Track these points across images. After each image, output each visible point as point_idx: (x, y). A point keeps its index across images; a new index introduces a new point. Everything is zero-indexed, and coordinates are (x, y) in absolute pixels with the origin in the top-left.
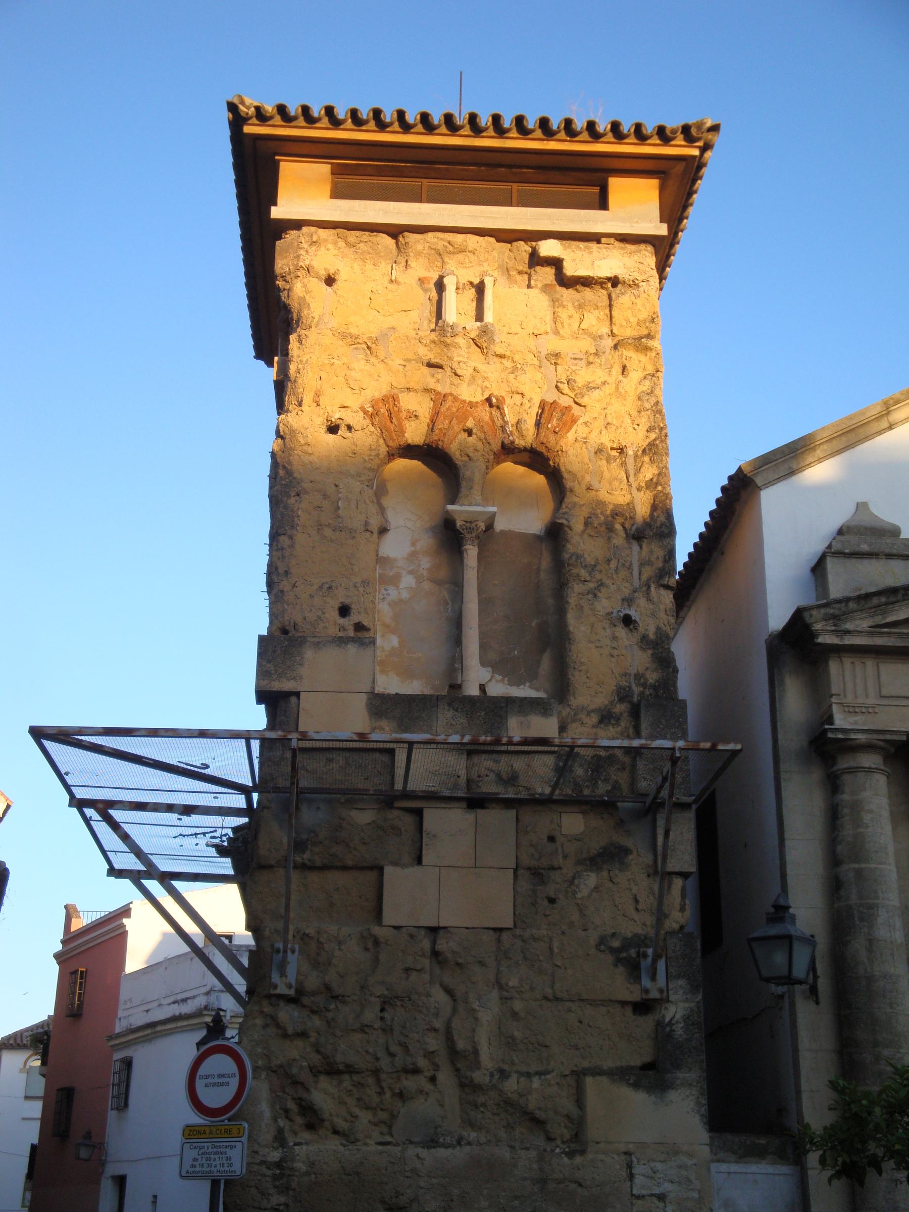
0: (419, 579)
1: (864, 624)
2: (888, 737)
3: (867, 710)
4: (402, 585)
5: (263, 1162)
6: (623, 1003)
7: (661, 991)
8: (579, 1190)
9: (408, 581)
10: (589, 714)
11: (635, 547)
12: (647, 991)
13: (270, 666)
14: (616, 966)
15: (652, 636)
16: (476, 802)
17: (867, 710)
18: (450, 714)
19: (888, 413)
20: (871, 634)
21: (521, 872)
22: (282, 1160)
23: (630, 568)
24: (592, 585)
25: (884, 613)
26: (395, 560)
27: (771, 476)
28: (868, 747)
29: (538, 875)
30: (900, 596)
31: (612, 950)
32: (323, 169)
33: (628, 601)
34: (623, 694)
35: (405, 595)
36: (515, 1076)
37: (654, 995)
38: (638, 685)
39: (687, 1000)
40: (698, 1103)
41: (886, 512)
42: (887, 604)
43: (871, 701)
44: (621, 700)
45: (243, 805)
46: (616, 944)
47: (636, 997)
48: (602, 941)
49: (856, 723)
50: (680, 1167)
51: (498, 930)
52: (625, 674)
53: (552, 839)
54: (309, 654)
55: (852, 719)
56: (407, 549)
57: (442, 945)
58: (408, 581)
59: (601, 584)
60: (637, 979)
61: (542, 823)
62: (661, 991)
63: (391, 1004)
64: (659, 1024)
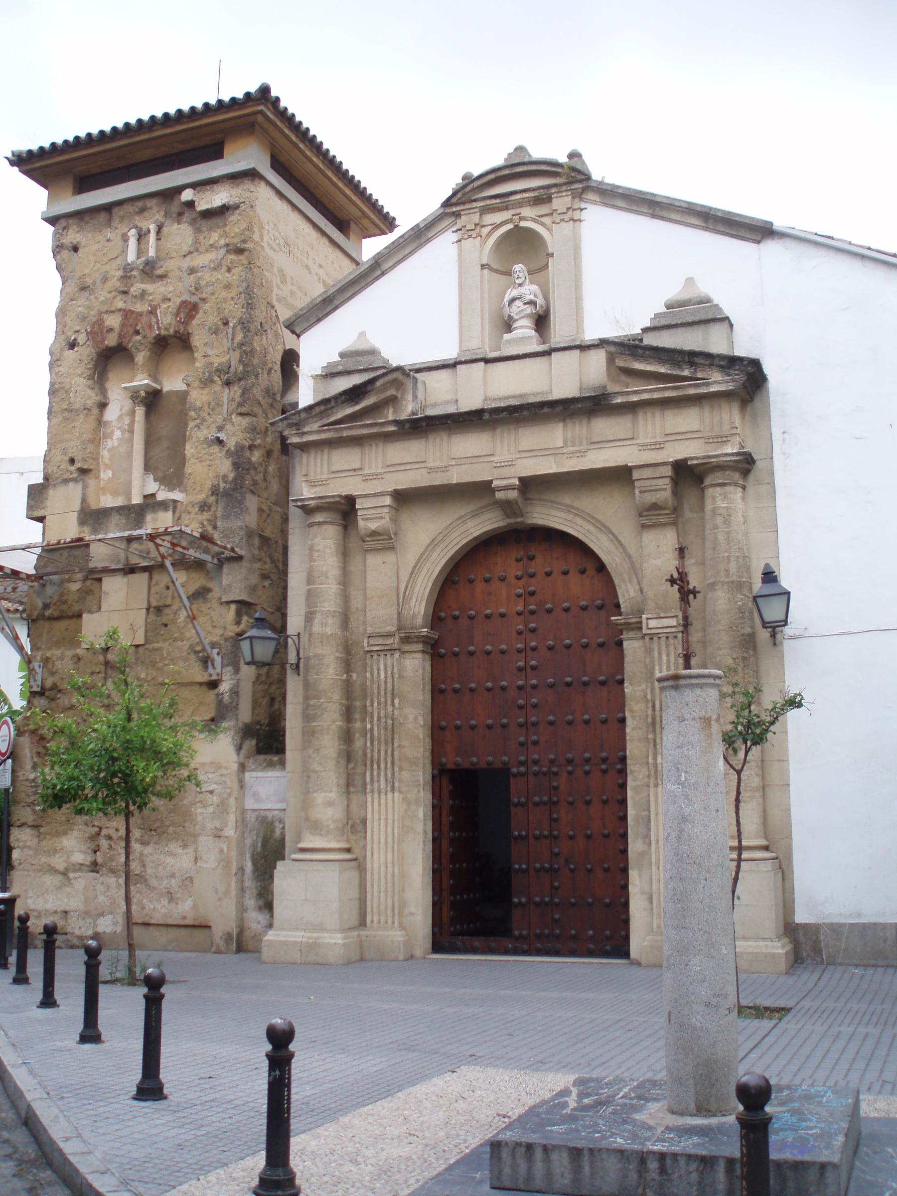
0: (123, 432)
1: (315, 426)
2: (328, 500)
3: (322, 483)
5: (27, 780)
6: (201, 684)
7: (218, 675)
9: (118, 434)
11: (227, 390)
12: (211, 675)
13: (33, 503)
16: (130, 570)
17: (322, 483)
18: (118, 517)
20: (318, 432)
21: (151, 609)
23: (222, 405)
25: (328, 416)
27: (306, 325)
30: (333, 403)
34: (215, 491)
37: (215, 677)
39: (232, 679)
40: (233, 739)
41: (376, 341)
42: (326, 410)
43: (325, 477)
44: (213, 494)
49: (315, 493)
50: (221, 775)
51: (137, 646)
55: (313, 490)
56: (118, 413)
57: (110, 656)
58: (118, 434)
59: (204, 420)
60: (206, 668)
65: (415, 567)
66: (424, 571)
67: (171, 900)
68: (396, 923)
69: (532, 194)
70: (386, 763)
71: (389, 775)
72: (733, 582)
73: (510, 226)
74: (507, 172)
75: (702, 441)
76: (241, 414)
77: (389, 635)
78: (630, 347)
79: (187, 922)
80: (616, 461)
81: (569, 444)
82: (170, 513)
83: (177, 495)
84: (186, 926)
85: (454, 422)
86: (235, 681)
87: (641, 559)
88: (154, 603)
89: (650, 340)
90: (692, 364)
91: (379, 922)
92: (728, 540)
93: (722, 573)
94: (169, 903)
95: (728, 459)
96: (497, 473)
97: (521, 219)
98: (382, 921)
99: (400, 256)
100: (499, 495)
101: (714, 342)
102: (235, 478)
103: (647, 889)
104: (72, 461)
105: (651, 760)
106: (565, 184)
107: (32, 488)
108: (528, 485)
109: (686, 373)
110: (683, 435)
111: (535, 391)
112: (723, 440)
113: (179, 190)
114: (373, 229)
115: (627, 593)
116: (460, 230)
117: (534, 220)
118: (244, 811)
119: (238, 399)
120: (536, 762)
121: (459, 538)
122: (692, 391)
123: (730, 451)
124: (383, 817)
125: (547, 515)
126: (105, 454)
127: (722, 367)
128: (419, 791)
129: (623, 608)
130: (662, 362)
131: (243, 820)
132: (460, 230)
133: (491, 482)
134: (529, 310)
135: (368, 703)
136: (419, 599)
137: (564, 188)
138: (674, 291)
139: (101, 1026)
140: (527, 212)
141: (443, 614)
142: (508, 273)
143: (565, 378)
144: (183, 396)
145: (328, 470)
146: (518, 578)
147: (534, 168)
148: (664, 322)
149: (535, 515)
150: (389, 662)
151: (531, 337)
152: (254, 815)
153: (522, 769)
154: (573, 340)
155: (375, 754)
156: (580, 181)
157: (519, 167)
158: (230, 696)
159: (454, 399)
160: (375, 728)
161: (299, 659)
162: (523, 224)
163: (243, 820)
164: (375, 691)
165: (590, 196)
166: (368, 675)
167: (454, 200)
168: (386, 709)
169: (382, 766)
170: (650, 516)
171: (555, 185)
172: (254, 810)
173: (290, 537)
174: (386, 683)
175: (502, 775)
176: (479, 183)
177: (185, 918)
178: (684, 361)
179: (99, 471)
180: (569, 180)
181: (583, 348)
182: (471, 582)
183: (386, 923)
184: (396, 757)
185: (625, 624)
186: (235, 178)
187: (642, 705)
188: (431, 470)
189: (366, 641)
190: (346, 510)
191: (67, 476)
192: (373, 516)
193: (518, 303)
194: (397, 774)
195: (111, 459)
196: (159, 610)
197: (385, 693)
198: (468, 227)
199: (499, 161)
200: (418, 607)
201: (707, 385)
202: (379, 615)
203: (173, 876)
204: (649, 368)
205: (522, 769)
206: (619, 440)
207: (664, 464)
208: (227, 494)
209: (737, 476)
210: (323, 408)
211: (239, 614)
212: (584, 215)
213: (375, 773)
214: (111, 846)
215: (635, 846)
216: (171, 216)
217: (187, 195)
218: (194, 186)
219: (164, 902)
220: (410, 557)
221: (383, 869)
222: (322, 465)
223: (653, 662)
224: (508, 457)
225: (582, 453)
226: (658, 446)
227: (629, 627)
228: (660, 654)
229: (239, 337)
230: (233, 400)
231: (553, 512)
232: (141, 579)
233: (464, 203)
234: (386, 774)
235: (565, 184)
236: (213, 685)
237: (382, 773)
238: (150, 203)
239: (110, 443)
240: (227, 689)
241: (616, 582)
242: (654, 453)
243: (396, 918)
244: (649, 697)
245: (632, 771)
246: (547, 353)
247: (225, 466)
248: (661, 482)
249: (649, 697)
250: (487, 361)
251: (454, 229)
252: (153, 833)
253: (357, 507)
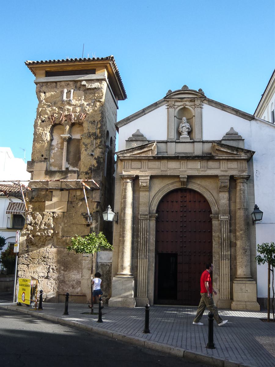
0: (58, 149)
6: (85, 225)
7: (91, 222)
8: (74, 255)
9: (56, 149)
10: (83, 173)
11: (95, 141)
12: (88, 222)
15: (97, 158)
16: (62, 190)
22: (27, 250)
23: (93, 145)
26: (54, 145)
27: (121, 125)
29: (71, 203)
31: (83, 215)
33: (93, 151)
34: (90, 169)
35: (55, 152)
36: (65, 237)
37: (90, 223)
41: (142, 132)
44: (90, 170)
46: (84, 214)
47: (87, 223)
53: (74, 196)
54: (35, 164)
56: (56, 143)
58: (56, 149)
60: (87, 220)
61: (73, 193)
62: (91, 222)
63: (216, 327)
64: (91, 228)
65: (154, 196)
66: (157, 198)
67: (73, 288)
68: (146, 296)
69: (189, 99)
73: (183, 107)
74: (183, 92)
75: (238, 171)
76: (100, 148)
77: (146, 215)
78: (219, 143)
79: (78, 294)
80: (214, 174)
81: (202, 168)
85: (170, 158)
86: (96, 225)
87: (219, 200)
88: (70, 200)
89: (223, 142)
90: (237, 151)
91: (141, 295)
92: (244, 197)
93: (243, 206)
94: (72, 289)
95: (245, 176)
96: (181, 173)
97: (186, 105)
98: (142, 295)
100: (182, 180)
101: (241, 145)
104: (42, 156)
106: (199, 98)
107: (28, 162)
109: (235, 153)
110: (233, 169)
112: (243, 171)
113: (81, 81)
114: (121, 98)
115: (214, 209)
116: (168, 105)
117: (189, 106)
118: (97, 263)
124: (143, 266)
125: (194, 186)
126: (52, 155)
127: (245, 152)
128: (153, 259)
129: (213, 212)
130: (229, 149)
131: (97, 265)
132: (168, 105)
133: (179, 175)
134: (187, 130)
136: (155, 206)
138: (227, 130)
139: (150, 329)
140: (187, 103)
143: (198, 149)
146: (181, 202)
147: (188, 92)
148: (226, 138)
149: (189, 186)
151: (188, 138)
152: (100, 264)
153: (181, 254)
154: (200, 140)
155: (141, 248)
156: (204, 98)
157: (185, 90)
158: (95, 229)
159: (166, 151)
160: (141, 241)
162: (186, 107)
163: (97, 265)
164: (142, 230)
165: (205, 102)
166: (140, 226)
167: (167, 97)
170: (221, 189)
171: (197, 98)
173: (115, 185)
174: (145, 228)
175: (175, 255)
176: (174, 94)
177: (78, 293)
178: (235, 150)
182: (168, 202)
183: (143, 296)
187: (217, 239)
188: (162, 171)
189: (139, 216)
192: (143, 182)
194: (147, 254)
196: (71, 203)
198: (171, 105)
200: (154, 208)
201: (241, 157)
203: (74, 281)
204: (225, 150)
205: (181, 254)
208: (94, 170)
209: (246, 180)
210: (131, 150)
211: (97, 205)
212: (203, 107)
213: (141, 253)
214: (53, 271)
216: (77, 88)
217: (84, 83)
219: (71, 288)
220: (153, 193)
221: (142, 281)
223: (221, 227)
224: (184, 169)
225: (206, 171)
226: (226, 171)
228: (223, 226)
230: (97, 144)
231: (194, 185)
232: (66, 193)
233: (170, 98)
234: (144, 254)
235: (199, 98)
236: (88, 225)
237: (143, 253)
239: (53, 151)
241: (211, 205)
242: (225, 173)
243: (146, 294)
244: (220, 236)
245: (214, 256)
247: (94, 162)
248: (226, 181)
249: (220, 236)
250: (176, 142)
251: (166, 105)
253: (140, 179)
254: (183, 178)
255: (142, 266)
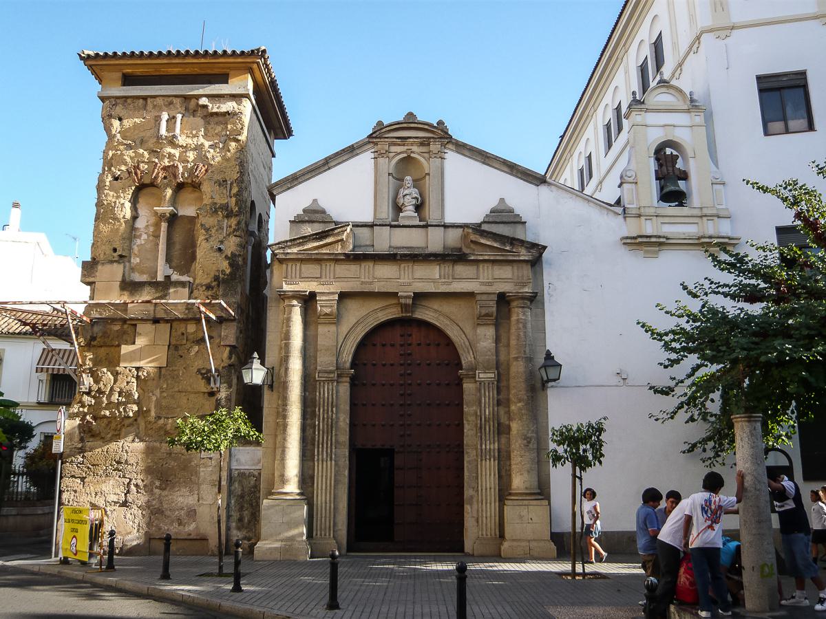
4: (142, 238)
6: (204, 393)
9: (144, 236)
10: (202, 286)
11: (226, 221)
12: (212, 388)
14: (202, 379)
16: (156, 321)
19: (328, 163)
22: (82, 447)
24: (207, 236)
27: (280, 190)
28: (294, 297)
29: (176, 348)
31: (201, 374)
32: (385, 124)
33: (222, 242)
34: (216, 278)
35: (143, 242)
36: (163, 418)
38: (222, 274)
41: (324, 204)
45: (510, 276)
46: (204, 371)
48: (199, 370)
52: (217, 271)
54: (100, 267)
58: (144, 236)
61: (181, 328)
65: (346, 335)
69: (419, 140)
70: (327, 444)
71: (329, 451)
72: (527, 357)
73: (405, 155)
74: (405, 125)
76: (235, 236)
77: (331, 372)
78: (477, 228)
81: (442, 277)
82: (187, 289)
83: (185, 278)
84: (191, 539)
87: (476, 342)
88: (174, 342)
89: (485, 227)
99: (340, 160)
100: (403, 301)
101: (519, 233)
102: (231, 273)
103: (475, 515)
104: (115, 250)
105: (479, 447)
107: (85, 264)
108: (418, 297)
109: (508, 248)
110: (502, 279)
111: (418, 246)
112: (524, 285)
115: (467, 359)
116: (377, 152)
117: (419, 154)
119: (234, 227)
120: (410, 446)
121: (373, 322)
122: (511, 258)
123: (527, 290)
125: (426, 314)
126: (135, 248)
127: (527, 248)
130: (495, 241)
131: (231, 474)
132: (377, 152)
133: (397, 293)
134: (414, 202)
135: (317, 410)
137: (437, 140)
138: (493, 203)
140: (415, 148)
141: (357, 362)
142: (402, 180)
143: (435, 241)
144: (192, 220)
145: (334, 276)
148: (491, 220)
150: (330, 387)
156: (447, 138)
157: (410, 122)
161: (273, 382)
162: (412, 155)
163: (231, 474)
165: (450, 146)
167: (374, 135)
168: (328, 413)
169: (325, 446)
170: (481, 320)
171: (433, 138)
172: (236, 469)
175: (390, 453)
179: (131, 257)
180: (439, 136)
181: (446, 226)
183: (325, 535)
184: (334, 441)
185: (466, 375)
186: (234, 97)
188: (363, 283)
189: (317, 374)
190: (308, 301)
191: (111, 258)
192: (325, 305)
193: (408, 197)
194: (334, 450)
195: (139, 251)
196: (176, 348)
197: (328, 404)
199: (401, 119)
202: (325, 361)
204: (488, 243)
206: (470, 279)
207: (494, 293)
208: (224, 281)
211: (231, 353)
213: (320, 449)
215: (468, 492)
216: (188, 111)
217: (203, 101)
218: (207, 96)
220: (344, 329)
222: (404, 273)
226: (490, 284)
227: (467, 376)
229: (235, 190)
230: (230, 227)
231: (427, 312)
238: (176, 100)
239: (138, 242)
240: (223, 397)
244: (479, 414)
246: (426, 226)
247: (225, 265)
248: (491, 303)
249: (479, 414)
250: (392, 226)
251: (373, 150)
252: (169, 483)
254: (406, 297)
255: (322, 476)
